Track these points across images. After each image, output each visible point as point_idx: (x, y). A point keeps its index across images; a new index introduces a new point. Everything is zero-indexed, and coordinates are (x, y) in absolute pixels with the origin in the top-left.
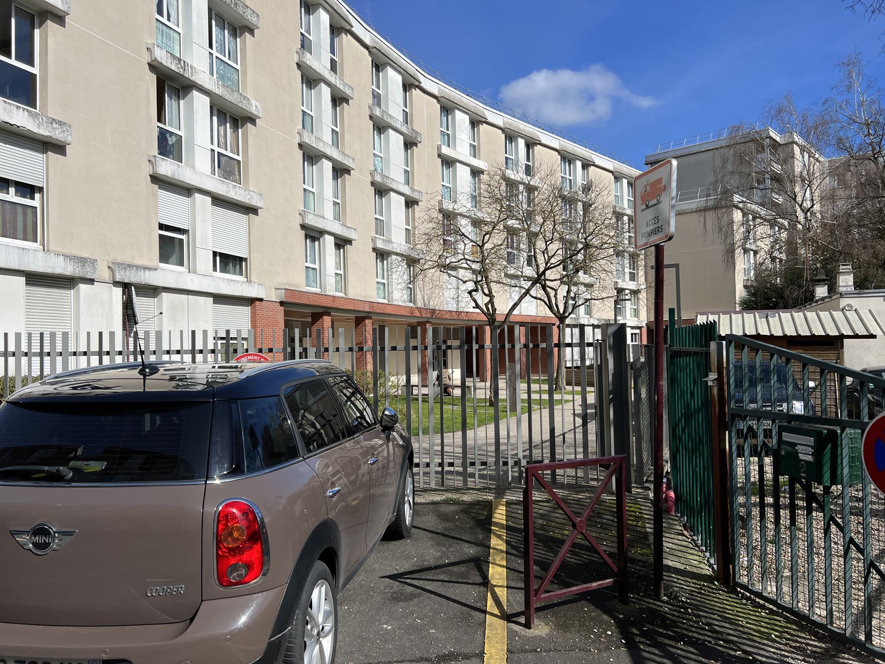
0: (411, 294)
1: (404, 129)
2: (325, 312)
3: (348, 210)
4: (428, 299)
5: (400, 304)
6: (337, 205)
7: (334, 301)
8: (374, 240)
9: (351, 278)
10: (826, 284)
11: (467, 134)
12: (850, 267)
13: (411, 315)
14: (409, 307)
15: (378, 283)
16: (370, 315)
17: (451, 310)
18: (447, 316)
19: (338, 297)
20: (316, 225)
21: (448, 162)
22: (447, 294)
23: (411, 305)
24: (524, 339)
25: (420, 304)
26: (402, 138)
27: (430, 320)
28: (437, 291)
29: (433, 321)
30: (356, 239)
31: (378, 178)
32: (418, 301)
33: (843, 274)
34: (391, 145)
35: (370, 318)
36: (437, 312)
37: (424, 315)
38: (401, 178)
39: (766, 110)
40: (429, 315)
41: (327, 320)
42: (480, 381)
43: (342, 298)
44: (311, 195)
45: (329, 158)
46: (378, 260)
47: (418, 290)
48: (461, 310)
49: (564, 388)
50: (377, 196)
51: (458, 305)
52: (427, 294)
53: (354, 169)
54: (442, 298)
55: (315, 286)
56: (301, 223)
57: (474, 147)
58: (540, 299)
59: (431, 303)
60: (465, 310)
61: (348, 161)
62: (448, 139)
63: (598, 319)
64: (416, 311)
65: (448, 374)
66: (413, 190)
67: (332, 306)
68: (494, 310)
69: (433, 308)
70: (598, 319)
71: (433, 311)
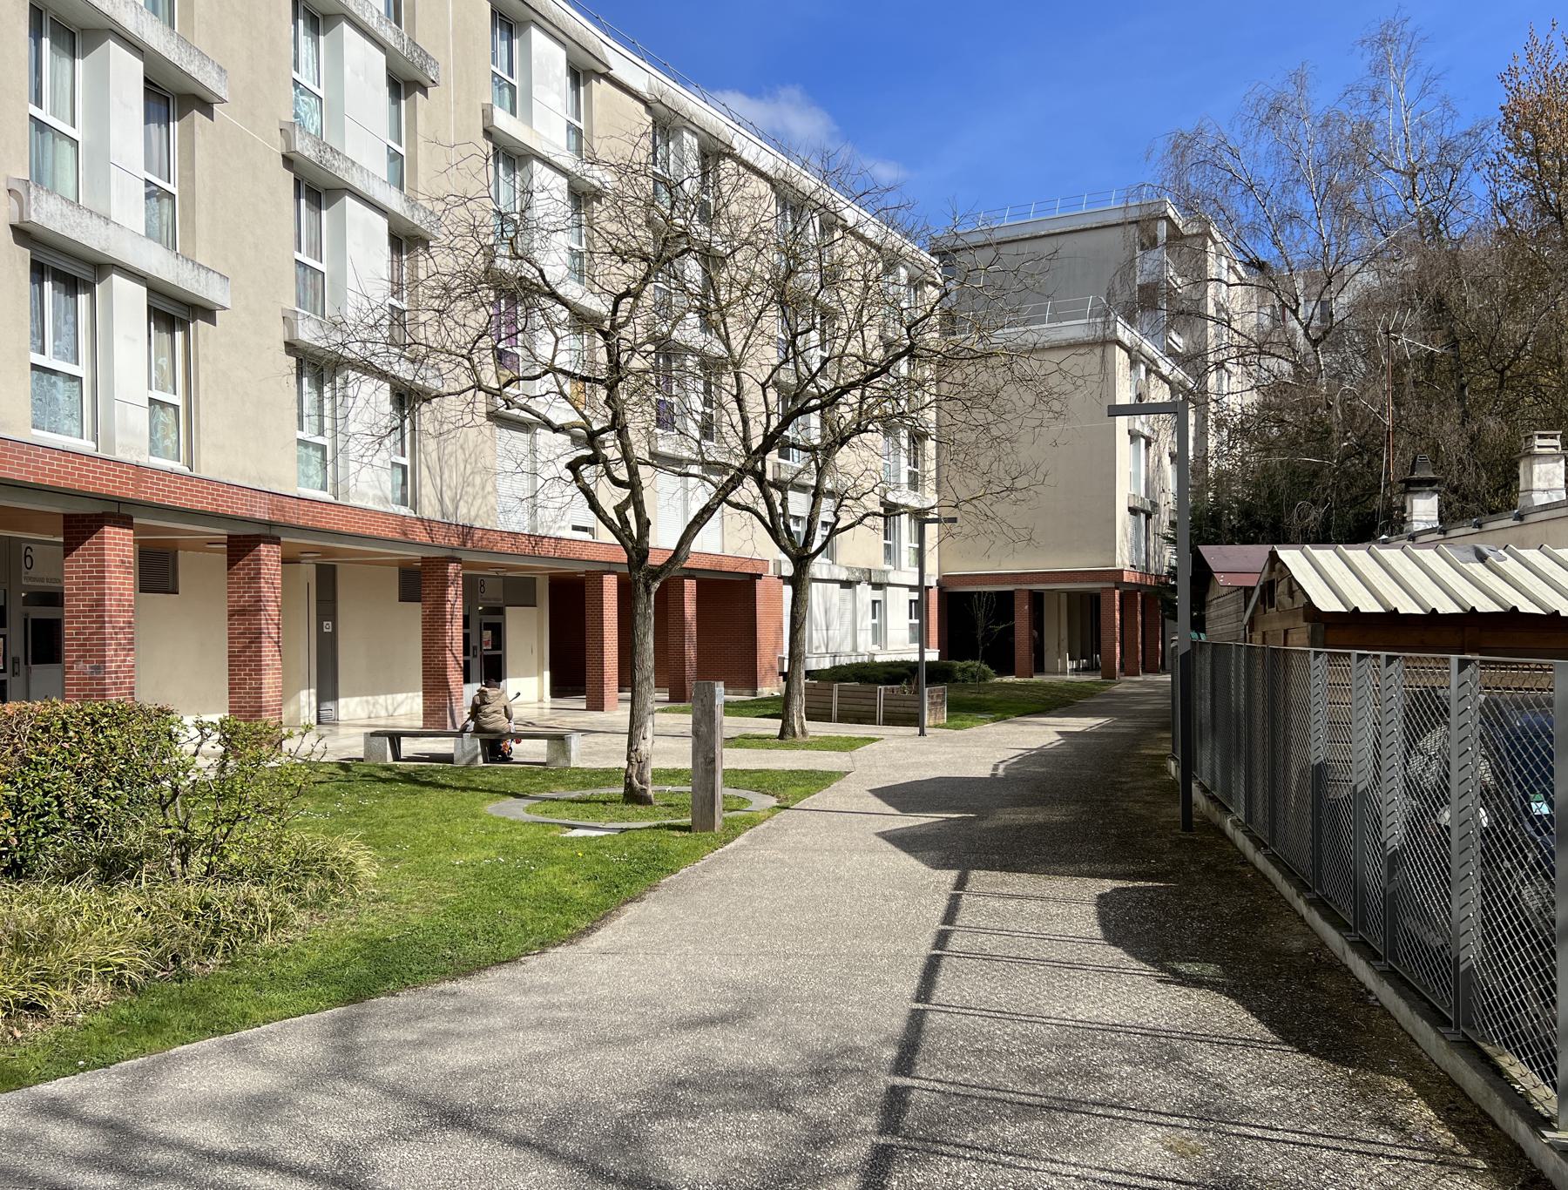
0: (404, 483)
1: (387, 33)
2: (111, 515)
3: (202, 220)
4: (453, 500)
5: (371, 505)
6: (166, 201)
7: (138, 481)
8: (288, 320)
9: (211, 419)
10: (1435, 491)
11: (559, 94)
12: (1557, 442)
13: (402, 538)
14: (396, 515)
15: (302, 443)
16: (275, 532)
17: (517, 530)
18: (505, 546)
19: (156, 471)
20: (73, 236)
21: (511, 156)
22: (504, 486)
23: (405, 511)
24: (694, 607)
25: (430, 510)
26: (380, 59)
27: (458, 555)
28: (478, 480)
29: (465, 557)
30: (228, 305)
31: (305, 148)
32: (425, 501)
33: (1541, 459)
34: (347, 69)
35: (275, 540)
36: (478, 534)
37: (440, 540)
38: (380, 167)
39: (1252, 101)
40: (455, 542)
41: (118, 544)
42: (589, 709)
43: (179, 475)
44: (68, 149)
45: (134, 45)
46: (305, 380)
47: (425, 471)
48: (540, 532)
49: (804, 733)
50: (303, 201)
51: (534, 514)
52: (449, 487)
53: (223, 101)
54: (491, 499)
55: (76, 431)
56: (16, 221)
57: (578, 132)
58: (748, 509)
59: (463, 510)
60: (551, 533)
61: (200, 68)
62: (513, 96)
63: (847, 568)
64: (419, 528)
65: (502, 702)
66: (412, 202)
67: (130, 495)
68: (644, 525)
69: (467, 522)
70: (847, 568)
71: (467, 531)
